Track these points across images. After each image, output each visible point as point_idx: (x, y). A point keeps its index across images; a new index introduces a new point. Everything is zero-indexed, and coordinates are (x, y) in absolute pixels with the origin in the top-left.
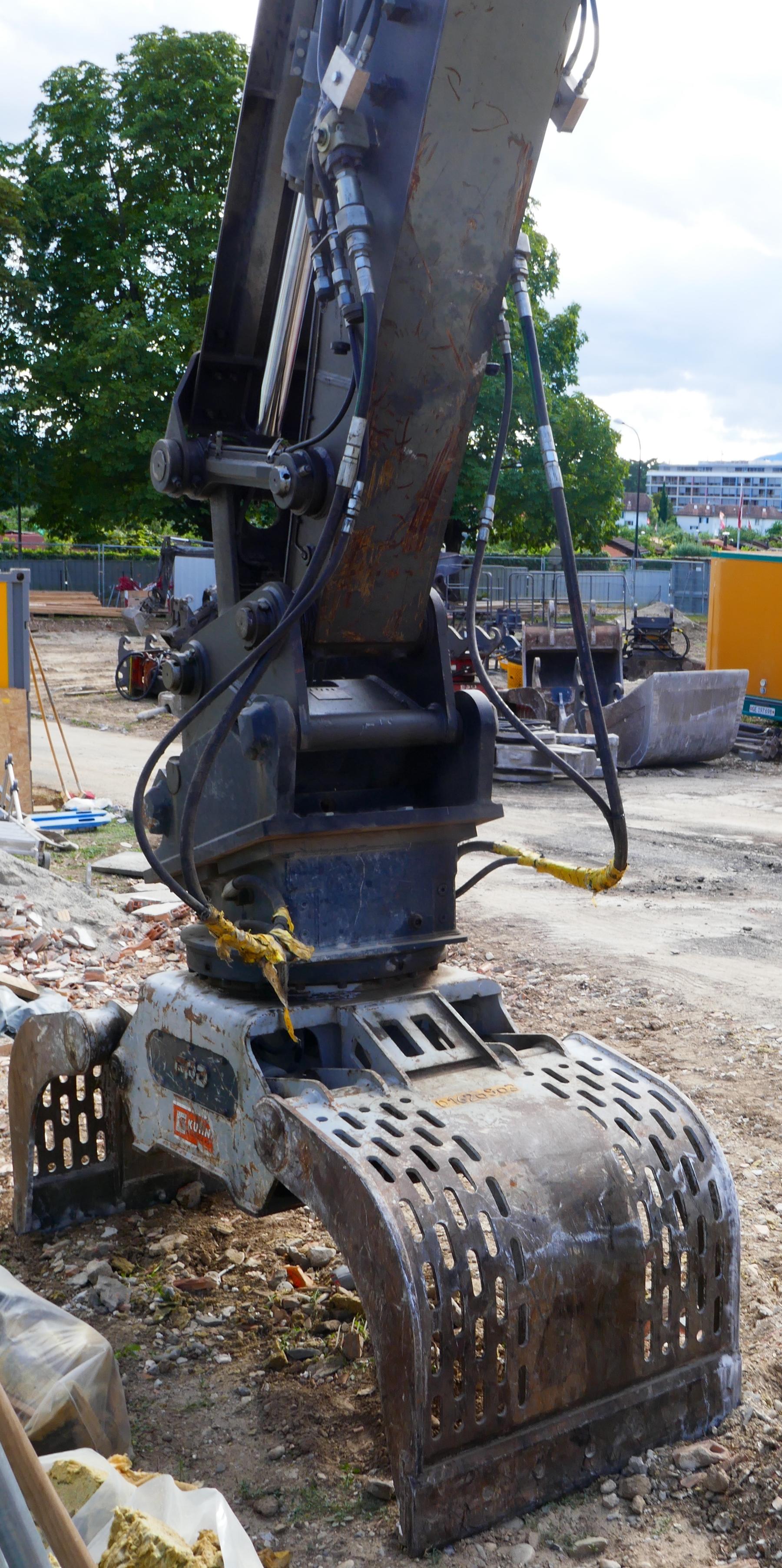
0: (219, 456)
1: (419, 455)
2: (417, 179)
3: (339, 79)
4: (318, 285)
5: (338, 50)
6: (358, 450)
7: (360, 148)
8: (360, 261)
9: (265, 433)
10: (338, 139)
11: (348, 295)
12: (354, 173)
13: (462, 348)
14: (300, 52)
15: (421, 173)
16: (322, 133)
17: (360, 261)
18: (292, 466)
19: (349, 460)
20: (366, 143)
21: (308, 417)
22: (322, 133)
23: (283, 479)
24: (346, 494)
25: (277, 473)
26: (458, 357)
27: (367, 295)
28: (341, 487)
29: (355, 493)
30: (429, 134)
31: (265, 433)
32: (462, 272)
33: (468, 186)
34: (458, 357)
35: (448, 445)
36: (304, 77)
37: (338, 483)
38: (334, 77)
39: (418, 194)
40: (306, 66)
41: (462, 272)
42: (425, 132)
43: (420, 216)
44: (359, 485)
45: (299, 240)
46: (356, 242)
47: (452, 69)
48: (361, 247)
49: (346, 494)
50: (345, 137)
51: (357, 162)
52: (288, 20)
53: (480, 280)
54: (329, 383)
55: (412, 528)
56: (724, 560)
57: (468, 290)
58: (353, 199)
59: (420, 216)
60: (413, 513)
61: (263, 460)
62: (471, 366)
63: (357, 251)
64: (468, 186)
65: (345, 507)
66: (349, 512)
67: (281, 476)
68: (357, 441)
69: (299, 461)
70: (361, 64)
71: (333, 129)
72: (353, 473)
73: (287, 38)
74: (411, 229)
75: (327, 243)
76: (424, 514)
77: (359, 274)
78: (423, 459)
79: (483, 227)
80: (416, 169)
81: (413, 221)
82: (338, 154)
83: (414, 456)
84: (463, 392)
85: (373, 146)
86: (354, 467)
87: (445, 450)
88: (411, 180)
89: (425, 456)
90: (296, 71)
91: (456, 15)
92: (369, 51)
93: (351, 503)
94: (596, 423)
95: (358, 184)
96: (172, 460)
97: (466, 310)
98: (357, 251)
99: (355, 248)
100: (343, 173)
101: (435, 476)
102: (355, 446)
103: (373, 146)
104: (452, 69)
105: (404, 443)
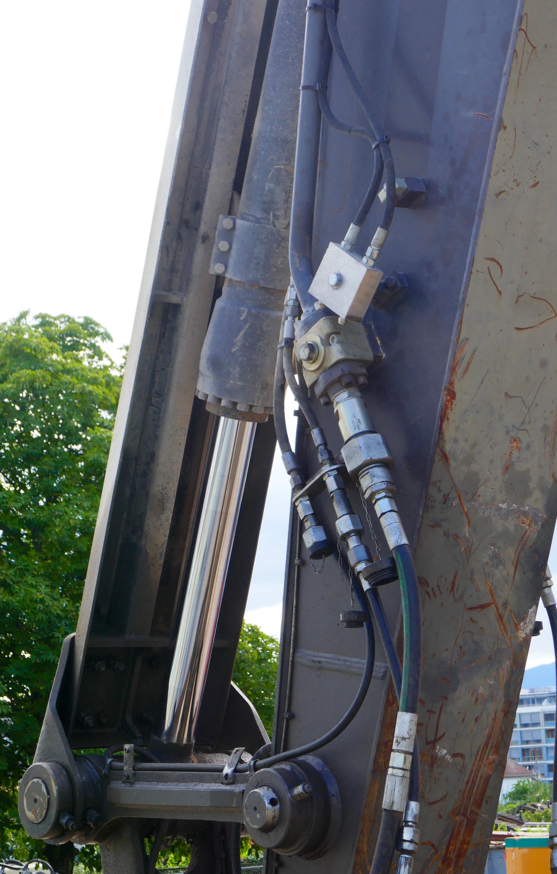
0: (129, 780)
1: (454, 755)
2: (452, 395)
3: (340, 281)
4: (311, 537)
5: (332, 248)
6: (410, 758)
7: (362, 362)
8: (383, 505)
9: (175, 740)
10: (336, 353)
11: (362, 548)
12: (359, 394)
13: (505, 604)
14: (223, 246)
15: (457, 388)
16: (312, 347)
17: (383, 505)
18: (283, 787)
19: (400, 773)
20: (369, 356)
21: (286, 715)
22: (312, 347)
23: (268, 805)
24: (396, 821)
25: (259, 798)
26: (501, 617)
27: (400, 548)
28: (391, 813)
29: (410, 818)
30: (467, 339)
31: (175, 740)
32: (504, 506)
33: (511, 397)
34: (501, 617)
35: (489, 737)
36: (228, 276)
37: (385, 804)
38: (333, 280)
39: (453, 415)
40: (231, 261)
41: (504, 506)
42: (462, 337)
43: (456, 441)
44: (414, 805)
45: (222, 476)
46: (376, 480)
47: (492, 259)
48: (384, 486)
49: (396, 821)
50: (345, 350)
51: (362, 380)
52: (198, 206)
53: (525, 514)
54: (319, 667)
55: (446, 860)
56: (525, 851)
57: (512, 528)
58: (363, 427)
59: (456, 441)
60: (448, 836)
61: (214, 780)
62: (517, 627)
63: (378, 492)
64: (511, 397)
65: (399, 839)
66: (406, 846)
67: (266, 802)
68: (407, 746)
69: (291, 780)
70: (371, 263)
71: (326, 342)
72: (406, 791)
73: (197, 229)
74: (445, 457)
75: (322, 483)
76: (461, 837)
77: (384, 521)
78: (459, 759)
79: (528, 447)
80: (451, 383)
81: (448, 447)
82: (337, 373)
83: (448, 757)
84: (508, 663)
85: (377, 358)
86: (407, 781)
87: (486, 744)
88: (443, 396)
89: (462, 756)
90: (217, 269)
91: (497, 196)
92: (382, 247)
93: (408, 834)
94: (265, 660)
95: (366, 406)
96: (59, 791)
97: (509, 554)
98: (378, 492)
99: (375, 489)
100: (344, 395)
101: (474, 782)
102: (406, 753)
103: (377, 358)
104: (492, 259)
105: (437, 739)
